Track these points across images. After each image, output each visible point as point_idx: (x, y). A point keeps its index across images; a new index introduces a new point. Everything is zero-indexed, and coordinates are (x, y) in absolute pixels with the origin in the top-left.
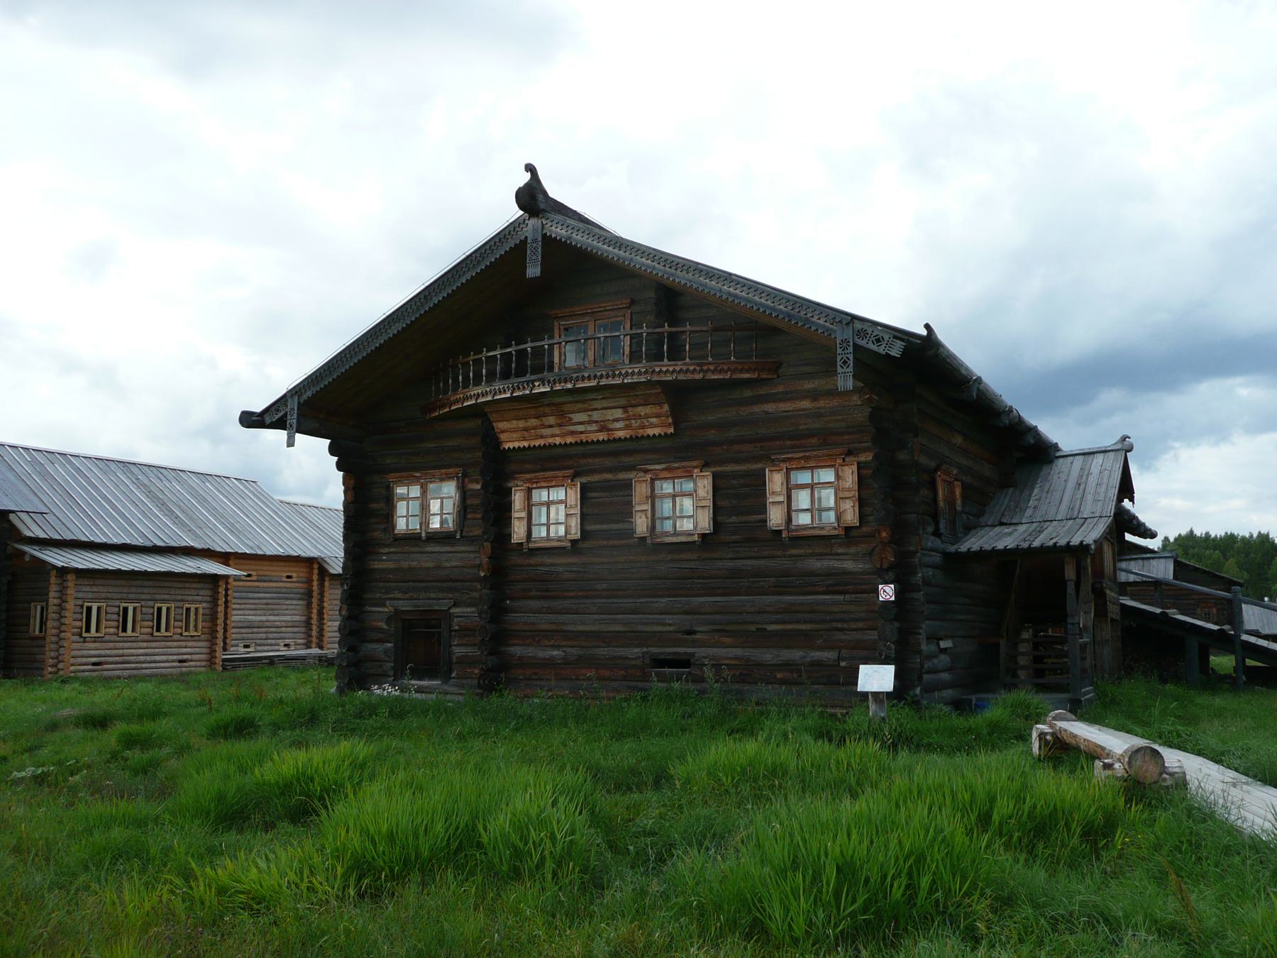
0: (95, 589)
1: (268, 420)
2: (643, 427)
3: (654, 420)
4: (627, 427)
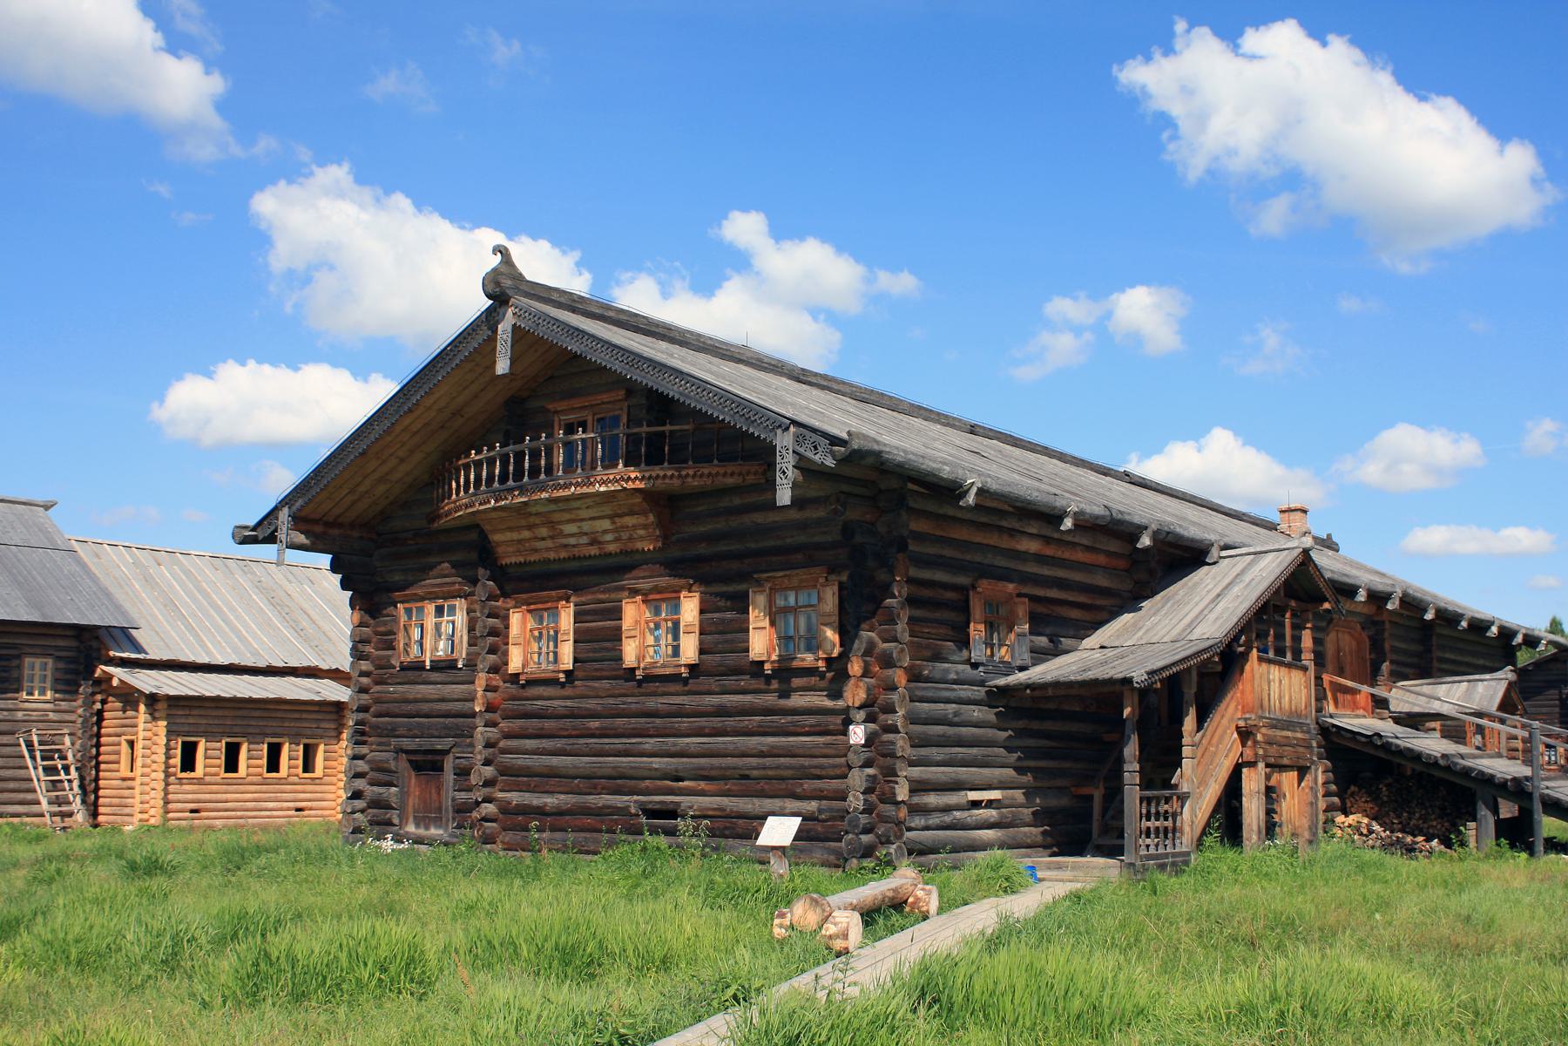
0: (191, 720)
1: (261, 534)
3: (641, 532)
4: (617, 540)
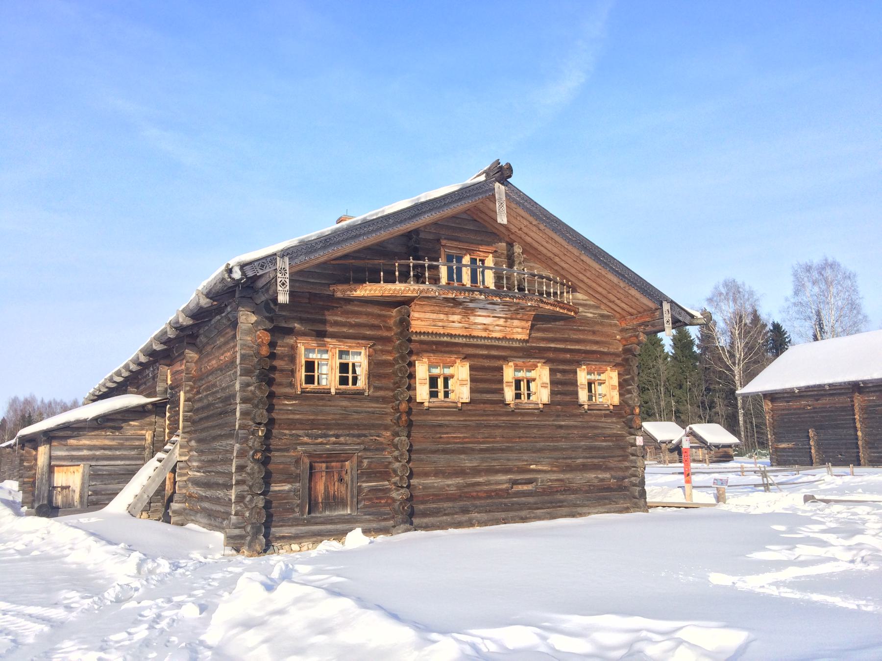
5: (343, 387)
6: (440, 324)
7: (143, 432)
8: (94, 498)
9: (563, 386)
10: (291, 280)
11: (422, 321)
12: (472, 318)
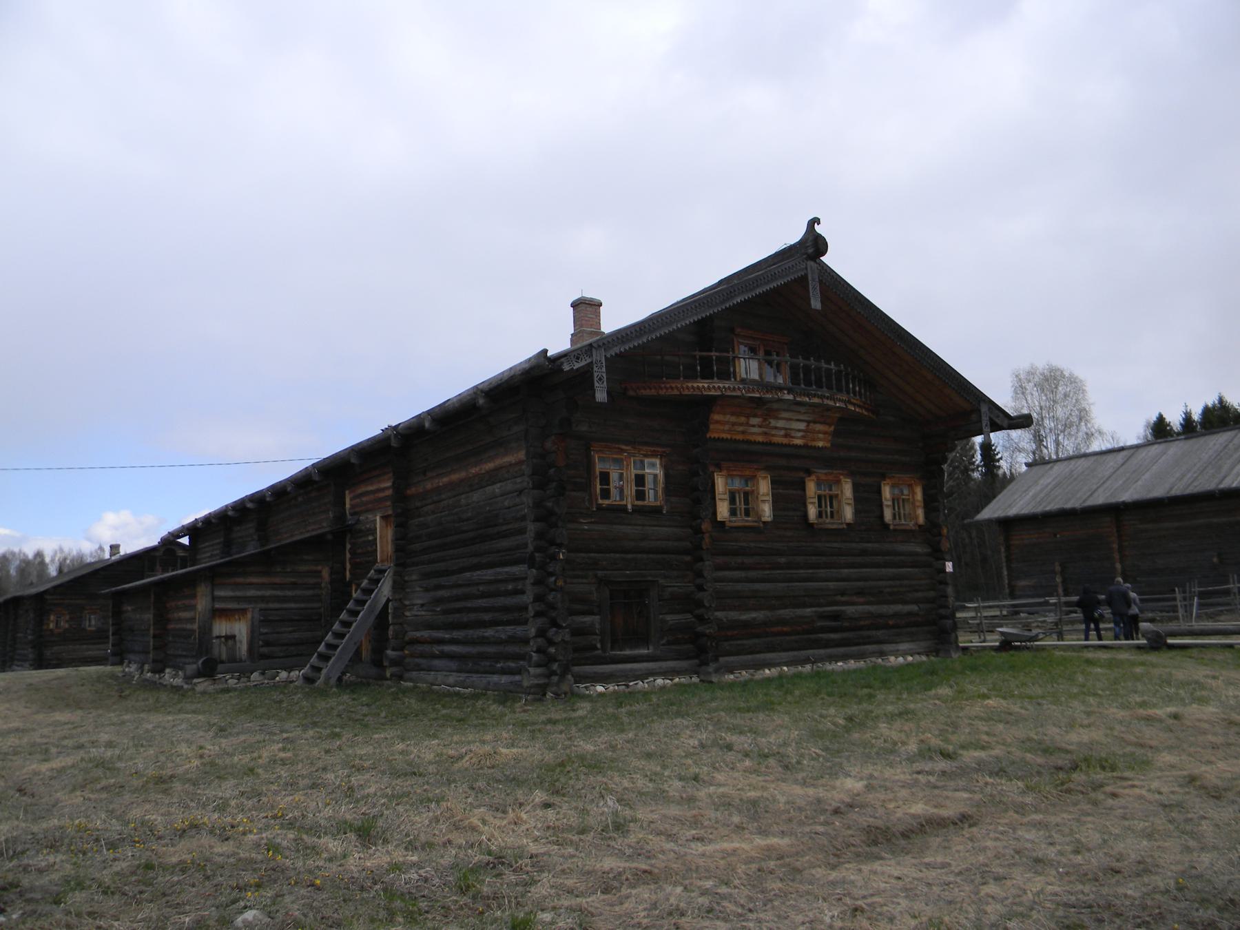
2: (813, 440)
4: (803, 437)
5: (640, 503)
6: (741, 429)
7: (319, 568)
8: (265, 650)
9: (868, 499)
10: (607, 373)
11: (722, 426)
12: (773, 423)
